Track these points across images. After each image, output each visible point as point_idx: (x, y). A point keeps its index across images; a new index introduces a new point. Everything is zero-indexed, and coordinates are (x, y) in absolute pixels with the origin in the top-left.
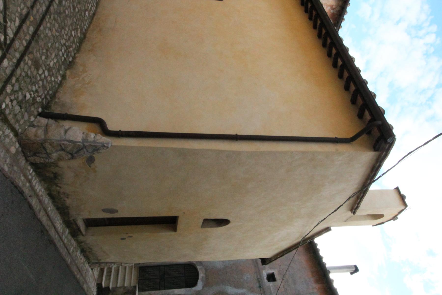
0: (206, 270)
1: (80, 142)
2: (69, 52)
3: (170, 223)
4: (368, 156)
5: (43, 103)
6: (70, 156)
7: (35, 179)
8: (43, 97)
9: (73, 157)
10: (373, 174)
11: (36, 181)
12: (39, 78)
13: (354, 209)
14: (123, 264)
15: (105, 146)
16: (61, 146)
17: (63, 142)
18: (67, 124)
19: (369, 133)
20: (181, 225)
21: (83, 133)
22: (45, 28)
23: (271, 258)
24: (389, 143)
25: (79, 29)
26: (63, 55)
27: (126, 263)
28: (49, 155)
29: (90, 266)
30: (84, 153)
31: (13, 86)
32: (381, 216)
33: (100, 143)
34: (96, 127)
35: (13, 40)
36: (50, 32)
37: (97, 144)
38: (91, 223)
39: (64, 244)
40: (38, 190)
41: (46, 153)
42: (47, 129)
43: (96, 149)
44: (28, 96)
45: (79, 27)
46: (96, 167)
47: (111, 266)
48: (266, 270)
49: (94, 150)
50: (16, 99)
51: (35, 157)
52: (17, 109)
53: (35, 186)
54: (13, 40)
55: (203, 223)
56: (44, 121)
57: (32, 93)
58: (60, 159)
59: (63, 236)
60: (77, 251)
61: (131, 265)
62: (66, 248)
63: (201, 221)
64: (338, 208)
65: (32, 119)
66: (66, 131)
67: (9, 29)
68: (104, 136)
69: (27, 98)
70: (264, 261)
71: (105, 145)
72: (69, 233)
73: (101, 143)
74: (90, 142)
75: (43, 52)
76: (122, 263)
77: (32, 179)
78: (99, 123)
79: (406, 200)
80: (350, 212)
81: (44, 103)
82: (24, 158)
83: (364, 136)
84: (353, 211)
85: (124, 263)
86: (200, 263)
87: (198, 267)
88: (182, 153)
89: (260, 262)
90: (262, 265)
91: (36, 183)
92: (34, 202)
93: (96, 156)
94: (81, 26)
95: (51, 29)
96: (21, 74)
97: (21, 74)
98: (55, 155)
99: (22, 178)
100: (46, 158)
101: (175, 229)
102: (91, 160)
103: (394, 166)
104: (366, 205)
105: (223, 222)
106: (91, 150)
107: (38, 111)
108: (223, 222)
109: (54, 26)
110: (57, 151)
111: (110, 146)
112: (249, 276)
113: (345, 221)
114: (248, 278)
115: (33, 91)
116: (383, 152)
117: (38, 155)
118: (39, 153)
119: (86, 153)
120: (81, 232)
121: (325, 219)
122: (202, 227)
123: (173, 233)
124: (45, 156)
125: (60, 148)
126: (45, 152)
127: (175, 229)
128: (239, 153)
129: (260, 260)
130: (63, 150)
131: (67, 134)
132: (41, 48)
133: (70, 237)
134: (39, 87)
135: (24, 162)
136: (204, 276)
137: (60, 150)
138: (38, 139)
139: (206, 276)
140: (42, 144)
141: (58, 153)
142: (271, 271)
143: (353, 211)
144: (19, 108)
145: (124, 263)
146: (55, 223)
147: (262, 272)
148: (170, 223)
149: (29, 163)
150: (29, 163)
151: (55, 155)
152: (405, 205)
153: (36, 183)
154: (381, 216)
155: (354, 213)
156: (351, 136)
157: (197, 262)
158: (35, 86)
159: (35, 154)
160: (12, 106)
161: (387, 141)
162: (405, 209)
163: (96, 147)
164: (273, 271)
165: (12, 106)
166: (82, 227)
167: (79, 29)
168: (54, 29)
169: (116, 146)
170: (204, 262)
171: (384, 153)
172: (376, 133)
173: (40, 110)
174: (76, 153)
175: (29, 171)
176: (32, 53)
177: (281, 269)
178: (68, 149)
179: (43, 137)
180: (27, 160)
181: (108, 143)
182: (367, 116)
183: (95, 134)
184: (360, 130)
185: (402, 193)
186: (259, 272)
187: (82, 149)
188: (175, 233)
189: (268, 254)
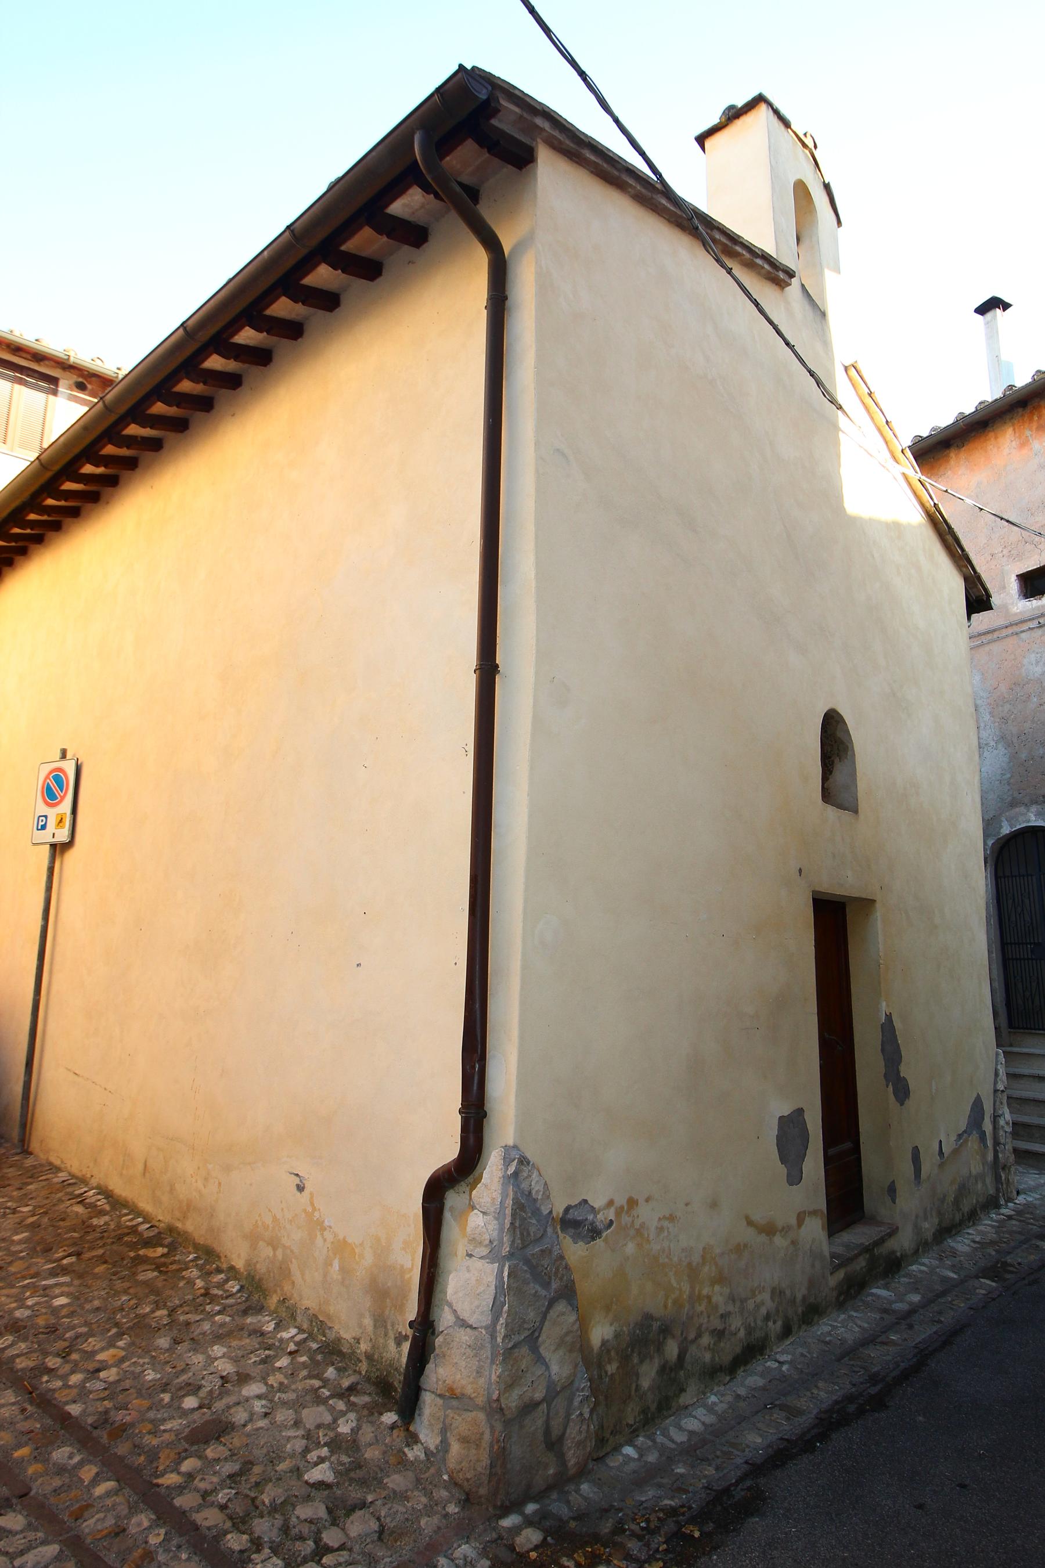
0: (1013, 804)
1: (500, 1272)
2: (206, 1294)
6: (561, 1306)
7: (665, 1434)
10: (631, 181)
11: (673, 1432)
13: (777, 274)
14: (1001, 1087)
18: (444, 1319)
20: (844, 883)
23: (966, 579)
29: (1010, 1200)
32: (801, 190)
34: (453, 1199)
37: (509, 1202)
39: (925, 1305)
40: (710, 1419)
42: (452, 1396)
44: (320, 1473)
45: (132, 1254)
46: (611, 1203)
47: (1009, 1129)
51: (568, 1443)
53: (691, 1433)
55: (840, 806)
56: (429, 1403)
57: (313, 1456)
59: (894, 1311)
62: (944, 1293)
64: (771, 322)
66: (463, 1324)
68: (479, 1180)
69: (329, 1477)
70: (978, 601)
71: (511, 1169)
72: (886, 1287)
73: (505, 1185)
74: (501, 1230)
76: (996, 1091)
78: (438, 1190)
79: (740, 103)
80: (787, 289)
83: (486, 211)
84: (782, 275)
85: (995, 1083)
86: (989, 824)
87: (1006, 830)
90: (989, 607)
94: (133, 1246)
95: (97, 1365)
96: (223, 1507)
97: (223, 1507)
98: (555, 1368)
102: (579, 1224)
103: (582, 74)
104: (759, 227)
105: (833, 728)
107: (393, 1427)
108: (833, 728)
109: (90, 1355)
112: (1033, 657)
113: (823, 314)
114: (1037, 662)
115: (307, 1450)
119: (542, 1245)
121: (812, 374)
124: (559, 1404)
129: (974, 616)
130: (533, 1340)
132: (151, 1415)
134: (297, 1424)
136: (1034, 808)
137: (535, 1349)
138: (487, 1436)
139: (1034, 802)
140: (507, 1423)
142: (1014, 586)
143: (782, 275)
144: (359, 1513)
145: (995, 1083)
147: (1016, 614)
148: (835, 921)
152: (759, 100)
153: (680, 1428)
154: (801, 190)
156: (481, 258)
157: (986, 836)
160: (342, 1547)
162: (770, 104)
164: (1014, 578)
165: (342, 1547)
167: (141, 1252)
168: (100, 1357)
170: (984, 812)
172: (465, 160)
173: (390, 1418)
176: (153, 1455)
177: (1005, 552)
179: (481, 1416)
182: (409, 204)
183: (473, 1208)
185: (715, 120)
186: (1017, 626)
188: (878, 905)
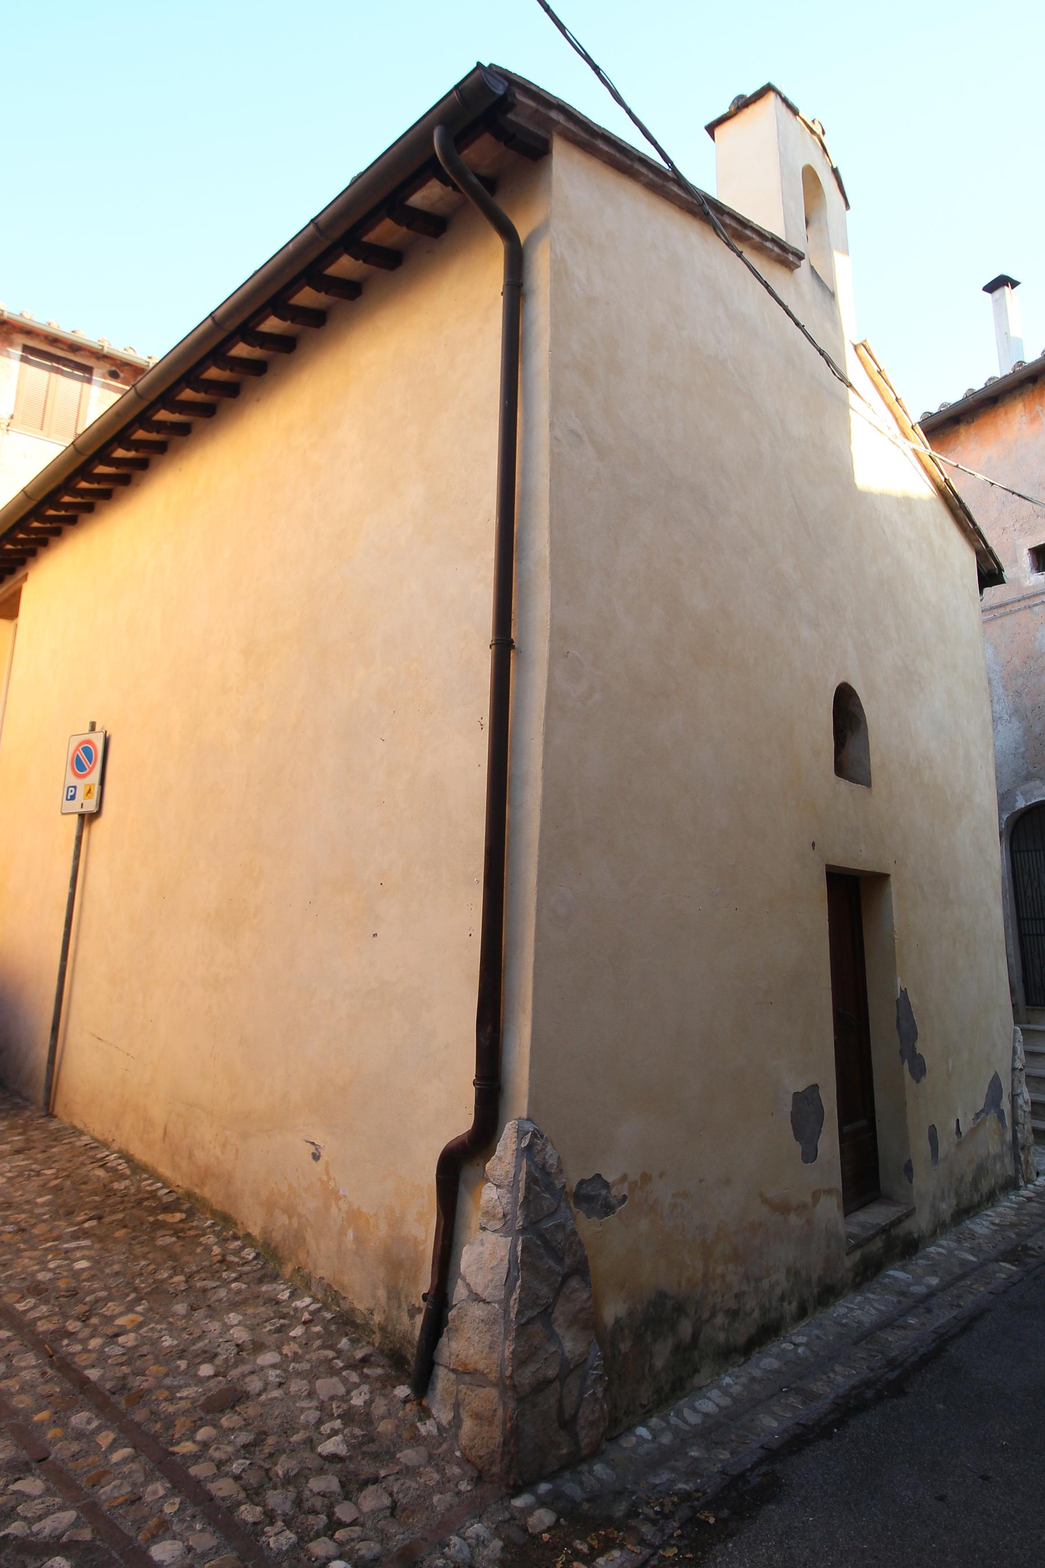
1: (514, 1246)
2: (222, 1261)
3: (853, 897)
4: (567, 170)
5: (378, 1378)
6: (574, 1283)
7: (679, 1414)
8: (354, 1377)
9: (581, 1270)
11: (687, 1413)
12: (276, 1393)
13: (786, 256)
15: (530, 1147)
16: (528, 1322)
17: (513, 1316)
19: (492, 184)
20: (860, 858)
21: (484, 1229)
22: (101, 1359)
23: (978, 553)
24: (508, 91)
25: (160, 1217)
26: (226, 1283)
27: (1014, 1052)
28: (569, 1369)
29: (1029, 1181)
30: (560, 1227)
31: (270, 1517)
32: (810, 175)
33: (518, 1168)
35: (91, 1511)
36: (121, 1339)
37: (523, 1175)
38: (865, 1176)
39: (943, 1288)
40: (725, 1401)
41: (562, 1377)
42: (465, 1373)
43: (539, 1182)
45: (151, 1219)
46: (624, 1178)
48: (1019, 568)
49: (549, 1187)
50: (330, 1500)
52: (371, 1500)
53: (706, 1415)
54: (91, 1511)
55: (852, 779)
58: (588, 1321)
60: (973, 1236)
61: (1020, 1036)
63: (844, 784)
65: (427, 1428)
67: (35, 1528)
69: (342, 1450)
70: (990, 575)
71: (525, 1143)
72: (903, 1269)
75: (185, 1373)
77: (676, 1431)
79: (749, 93)
80: (797, 271)
81: (380, 1371)
82: (584, 1467)
83: (500, 202)
85: (1014, 1061)
86: (1004, 798)
87: (1021, 804)
88: (558, 848)
89: (993, 593)
91: (695, 1410)
92: (771, 1424)
93: (572, 1178)
94: (152, 1211)
96: (237, 1478)
97: (237, 1478)
98: (568, 1345)
99: (663, 1477)
100: (584, 1378)
101: (878, 880)
102: (594, 1197)
104: (767, 209)
105: (846, 709)
106: (547, 1200)
107: (406, 1401)
108: (846, 709)
110: (552, 1337)
111: (529, 1127)
113: (833, 295)
115: (320, 1422)
116: (552, 120)
117: (568, 1412)
118: (560, 1411)
120: (899, 1221)
121: (822, 353)
122: (867, 782)
123: (894, 885)
125: (538, 1326)
126: (557, 1384)
127: (878, 880)
128: (558, 633)
129: (986, 590)
130: (546, 1314)
131: (485, 1295)
132: (168, 1381)
133: (920, 1263)
135: (598, 1468)
137: (548, 1324)
138: (500, 1412)
140: (520, 1400)
141: (559, 1331)
144: (371, 1488)
145: (1014, 1061)
146: (860, 1323)
147: (1029, 588)
148: (853, 897)
149: (604, 1445)
150: (604, 1445)
151: (571, 1344)
152: (768, 89)
153: (695, 1410)
154: (810, 175)
155: (800, 257)
157: (1001, 810)
158: (302, 1410)
159: (567, 1424)
160: (354, 1523)
161: (504, 97)
162: (778, 93)
163: (531, 1180)
164: (1026, 551)
165: (354, 1523)
166: (876, 1215)
167: (160, 1217)
169: (533, 1102)
171: (554, 115)
172: (482, 153)
174: (560, 1260)
175: (641, 1439)
178: (545, 1290)
180: (596, 1453)
181: (521, 1134)
182: (428, 196)
183: (487, 1180)
184: (481, 215)
185: (724, 110)
187: (541, 1236)
188: (892, 879)
189: (966, 561)
